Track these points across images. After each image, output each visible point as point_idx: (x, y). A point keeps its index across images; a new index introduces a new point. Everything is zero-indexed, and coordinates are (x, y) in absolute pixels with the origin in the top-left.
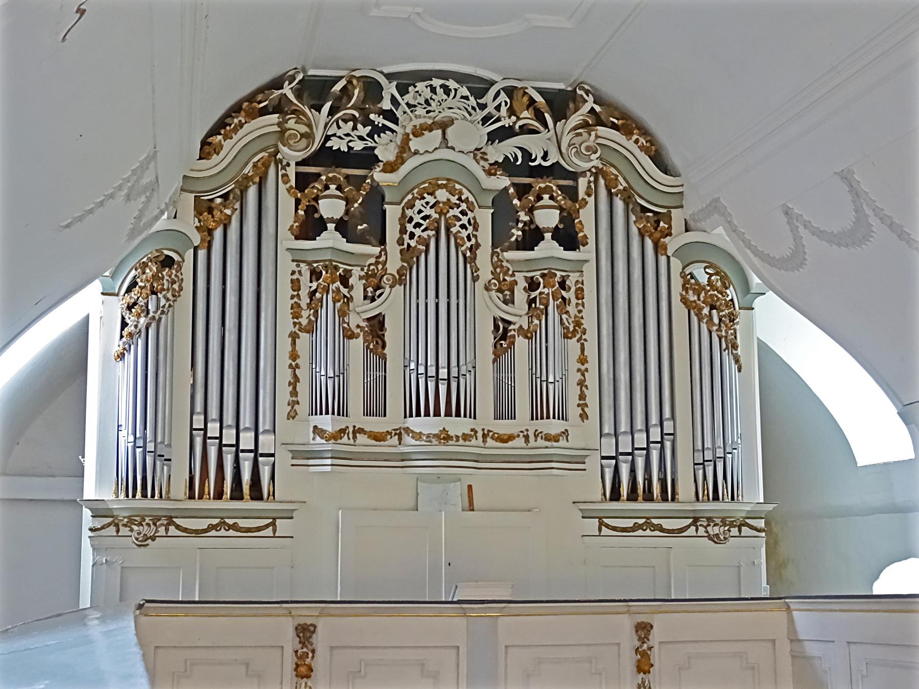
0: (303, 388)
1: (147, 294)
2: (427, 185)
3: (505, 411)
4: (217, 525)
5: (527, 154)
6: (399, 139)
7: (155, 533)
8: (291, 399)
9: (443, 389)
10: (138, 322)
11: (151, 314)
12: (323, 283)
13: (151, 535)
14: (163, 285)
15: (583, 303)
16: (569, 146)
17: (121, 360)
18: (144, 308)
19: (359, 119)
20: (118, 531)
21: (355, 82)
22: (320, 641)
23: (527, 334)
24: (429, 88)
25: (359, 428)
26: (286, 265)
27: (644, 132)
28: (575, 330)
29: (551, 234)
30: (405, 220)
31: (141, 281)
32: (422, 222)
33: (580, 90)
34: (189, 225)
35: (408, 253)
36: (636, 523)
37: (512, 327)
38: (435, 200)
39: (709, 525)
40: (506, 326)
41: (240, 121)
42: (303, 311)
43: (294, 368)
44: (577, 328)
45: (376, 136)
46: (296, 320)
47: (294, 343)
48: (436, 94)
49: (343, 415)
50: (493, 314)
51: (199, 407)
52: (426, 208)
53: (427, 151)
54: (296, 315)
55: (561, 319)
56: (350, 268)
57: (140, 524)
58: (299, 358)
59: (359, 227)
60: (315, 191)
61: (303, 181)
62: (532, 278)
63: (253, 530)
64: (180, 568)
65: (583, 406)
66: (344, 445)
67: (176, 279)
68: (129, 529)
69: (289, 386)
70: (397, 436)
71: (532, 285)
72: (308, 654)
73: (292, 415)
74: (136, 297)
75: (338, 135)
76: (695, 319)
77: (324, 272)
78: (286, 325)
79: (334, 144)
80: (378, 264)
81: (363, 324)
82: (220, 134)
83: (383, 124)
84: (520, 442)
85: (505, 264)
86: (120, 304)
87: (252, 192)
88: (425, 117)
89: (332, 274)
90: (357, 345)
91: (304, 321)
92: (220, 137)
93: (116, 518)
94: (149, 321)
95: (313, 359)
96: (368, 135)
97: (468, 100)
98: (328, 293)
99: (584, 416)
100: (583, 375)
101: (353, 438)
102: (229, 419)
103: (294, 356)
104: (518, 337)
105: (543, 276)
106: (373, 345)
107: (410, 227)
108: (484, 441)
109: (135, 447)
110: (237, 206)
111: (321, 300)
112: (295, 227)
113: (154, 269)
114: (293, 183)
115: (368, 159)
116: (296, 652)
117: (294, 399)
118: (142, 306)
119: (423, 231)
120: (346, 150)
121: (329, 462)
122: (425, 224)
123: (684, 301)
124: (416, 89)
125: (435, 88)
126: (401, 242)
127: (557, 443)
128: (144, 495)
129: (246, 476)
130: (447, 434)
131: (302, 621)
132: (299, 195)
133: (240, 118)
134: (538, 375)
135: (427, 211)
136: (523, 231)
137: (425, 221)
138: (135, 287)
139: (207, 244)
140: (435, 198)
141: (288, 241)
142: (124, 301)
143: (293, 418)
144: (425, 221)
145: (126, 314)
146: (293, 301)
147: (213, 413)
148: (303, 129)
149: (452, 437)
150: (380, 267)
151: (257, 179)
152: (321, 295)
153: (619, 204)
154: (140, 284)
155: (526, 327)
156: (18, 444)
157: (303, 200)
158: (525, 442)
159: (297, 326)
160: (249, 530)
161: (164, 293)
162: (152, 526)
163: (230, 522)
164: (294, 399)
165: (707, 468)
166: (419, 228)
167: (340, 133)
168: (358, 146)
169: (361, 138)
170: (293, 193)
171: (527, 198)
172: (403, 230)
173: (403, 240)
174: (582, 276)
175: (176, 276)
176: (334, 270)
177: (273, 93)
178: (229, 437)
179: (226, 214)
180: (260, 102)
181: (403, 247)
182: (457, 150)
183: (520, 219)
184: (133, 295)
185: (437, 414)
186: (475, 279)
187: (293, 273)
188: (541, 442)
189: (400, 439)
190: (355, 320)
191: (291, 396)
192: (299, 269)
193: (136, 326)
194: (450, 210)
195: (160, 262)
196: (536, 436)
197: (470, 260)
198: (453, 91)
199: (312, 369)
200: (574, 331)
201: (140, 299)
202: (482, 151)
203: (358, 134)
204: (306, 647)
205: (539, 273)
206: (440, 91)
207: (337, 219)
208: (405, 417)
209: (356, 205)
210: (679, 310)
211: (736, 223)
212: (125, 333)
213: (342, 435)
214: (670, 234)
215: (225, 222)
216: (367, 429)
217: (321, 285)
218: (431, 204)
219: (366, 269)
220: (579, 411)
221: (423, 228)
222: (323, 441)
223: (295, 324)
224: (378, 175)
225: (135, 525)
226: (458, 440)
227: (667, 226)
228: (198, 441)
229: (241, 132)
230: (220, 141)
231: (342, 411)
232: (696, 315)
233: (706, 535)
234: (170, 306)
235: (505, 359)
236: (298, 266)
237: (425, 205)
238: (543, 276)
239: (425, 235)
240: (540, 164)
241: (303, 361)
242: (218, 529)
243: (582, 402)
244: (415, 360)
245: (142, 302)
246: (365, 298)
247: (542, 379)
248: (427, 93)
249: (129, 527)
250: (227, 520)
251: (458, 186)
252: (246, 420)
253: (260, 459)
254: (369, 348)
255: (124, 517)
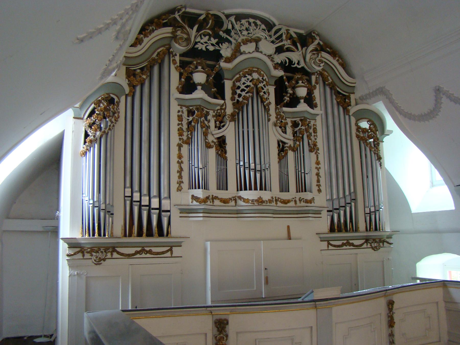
0: (185, 174)
1: (101, 118)
2: (247, 70)
3: (284, 188)
4: (140, 251)
5: (291, 62)
6: (233, 46)
7: (105, 257)
8: (179, 180)
9: (258, 175)
10: (96, 134)
11: (103, 130)
12: (195, 117)
13: (104, 257)
14: (110, 113)
15: (317, 135)
16: (310, 59)
17: (84, 156)
18: (99, 126)
19: (212, 35)
20: (83, 256)
21: (210, 16)
22: (231, 329)
23: (294, 149)
24: (247, 22)
25: (215, 196)
26: (175, 108)
27: (340, 57)
28: (314, 148)
29: (303, 100)
30: (234, 88)
31: (98, 111)
32: (245, 89)
33: (313, 33)
34: (124, 83)
35: (238, 105)
36: (343, 243)
37: (286, 145)
38: (252, 78)
39: (372, 242)
40: (283, 144)
41: (153, 28)
42: (184, 132)
43: (180, 163)
44: (315, 147)
45: (220, 44)
46: (180, 137)
47: (180, 150)
48: (251, 26)
49: (207, 190)
50: (277, 138)
51: (128, 184)
52: (247, 82)
53: (249, 53)
54: (181, 134)
55: (309, 142)
56: (208, 111)
57: (97, 252)
58: (183, 158)
59: (213, 90)
60: (191, 69)
61: (183, 65)
62: (295, 121)
63: (160, 253)
64: (120, 276)
65: (319, 186)
66: (208, 206)
67: (116, 111)
68: (90, 254)
69: (177, 173)
70: (234, 201)
71: (295, 124)
72: (224, 338)
73: (179, 189)
74: (95, 120)
75: (201, 42)
76: (363, 145)
77: (196, 112)
78: (175, 139)
79: (199, 46)
80: (222, 110)
81: (215, 141)
82: (142, 34)
83: (226, 37)
84: (292, 204)
85: (282, 114)
86: (84, 124)
87: (156, 69)
88: (246, 36)
89: (201, 113)
90: (212, 152)
91: (185, 138)
92: (142, 36)
93: (83, 248)
94: (102, 134)
95: (190, 157)
96: (216, 43)
97: (265, 31)
98: (198, 124)
99: (319, 191)
100: (318, 170)
101: (212, 202)
102: (145, 191)
103: (180, 156)
104: (289, 150)
105: (301, 120)
106: (220, 152)
107: (238, 91)
108: (276, 203)
109: (94, 207)
110: (149, 74)
111: (194, 127)
112: (179, 88)
113: (105, 104)
114: (178, 64)
115: (217, 56)
116: (216, 337)
117: (181, 180)
118: (98, 125)
119: (246, 93)
120: (205, 50)
121: (201, 215)
122: (247, 90)
123: (358, 136)
124: (241, 23)
125: (251, 23)
126: (233, 99)
127: (311, 204)
128: (100, 235)
129: (155, 223)
130: (262, 200)
131: (218, 317)
132: (182, 70)
133: (153, 27)
134: (300, 170)
135: (248, 83)
136: (289, 97)
137: (247, 88)
138: (94, 114)
139: (132, 94)
140: (252, 77)
141: (175, 94)
142: (87, 122)
143: (180, 190)
144: (247, 88)
145: (88, 129)
146: (179, 127)
147: (136, 188)
148: (185, 36)
149: (264, 201)
150: (223, 111)
151: (160, 61)
152: (194, 124)
153: (328, 89)
154: (97, 112)
155: (292, 146)
156: (355, 285)
157: (184, 73)
158: (295, 204)
159: (181, 141)
160: (158, 253)
161: (110, 118)
162: (104, 253)
163: (147, 249)
164: (181, 180)
165: (372, 215)
166: (244, 92)
167: (202, 41)
168: (211, 48)
169: (212, 45)
170: (179, 69)
171: (292, 82)
172: (234, 93)
173: (235, 98)
174: (316, 122)
175: (116, 109)
176: (202, 111)
177: (170, 16)
178: (145, 201)
179: (143, 78)
180: (163, 20)
181: (234, 102)
182: (263, 53)
183: (288, 92)
184: (92, 118)
185: (256, 189)
186: (269, 120)
187: (179, 111)
188: (303, 204)
189: (236, 202)
190: (211, 138)
191: (179, 179)
192: (182, 110)
193: (94, 136)
194: (260, 84)
195: (108, 100)
196: (300, 201)
197: (267, 110)
198: (259, 26)
199: (190, 164)
200: (313, 148)
201: (97, 120)
202: (272, 57)
203: (211, 42)
204: (223, 334)
205: (298, 119)
206: (253, 25)
207: (203, 84)
208: (238, 190)
209: (211, 78)
210: (356, 142)
211: (394, 98)
212: (88, 140)
213: (208, 200)
214: (350, 105)
215: (142, 82)
216: (220, 197)
217: (195, 118)
218: (250, 80)
219: (216, 111)
220: (317, 188)
221: (246, 92)
222: (198, 204)
223: (180, 139)
224: (223, 64)
225: (94, 252)
226: (267, 203)
227: (349, 101)
228: (128, 203)
229: (153, 35)
230: (142, 37)
231: (206, 187)
232: (364, 143)
233: (370, 247)
234: (114, 126)
235: (283, 161)
236: (181, 108)
237: (247, 80)
238: (301, 120)
239: (247, 95)
240: (296, 67)
241: (185, 159)
242: (141, 253)
243: (318, 184)
244: (243, 160)
245: (98, 122)
246: (216, 127)
247: (302, 172)
248: (247, 25)
249: (90, 253)
250: (146, 248)
251: (262, 73)
252: (154, 192)
253: (163, 213)
254: (218, 153)
255: (88, 248)
